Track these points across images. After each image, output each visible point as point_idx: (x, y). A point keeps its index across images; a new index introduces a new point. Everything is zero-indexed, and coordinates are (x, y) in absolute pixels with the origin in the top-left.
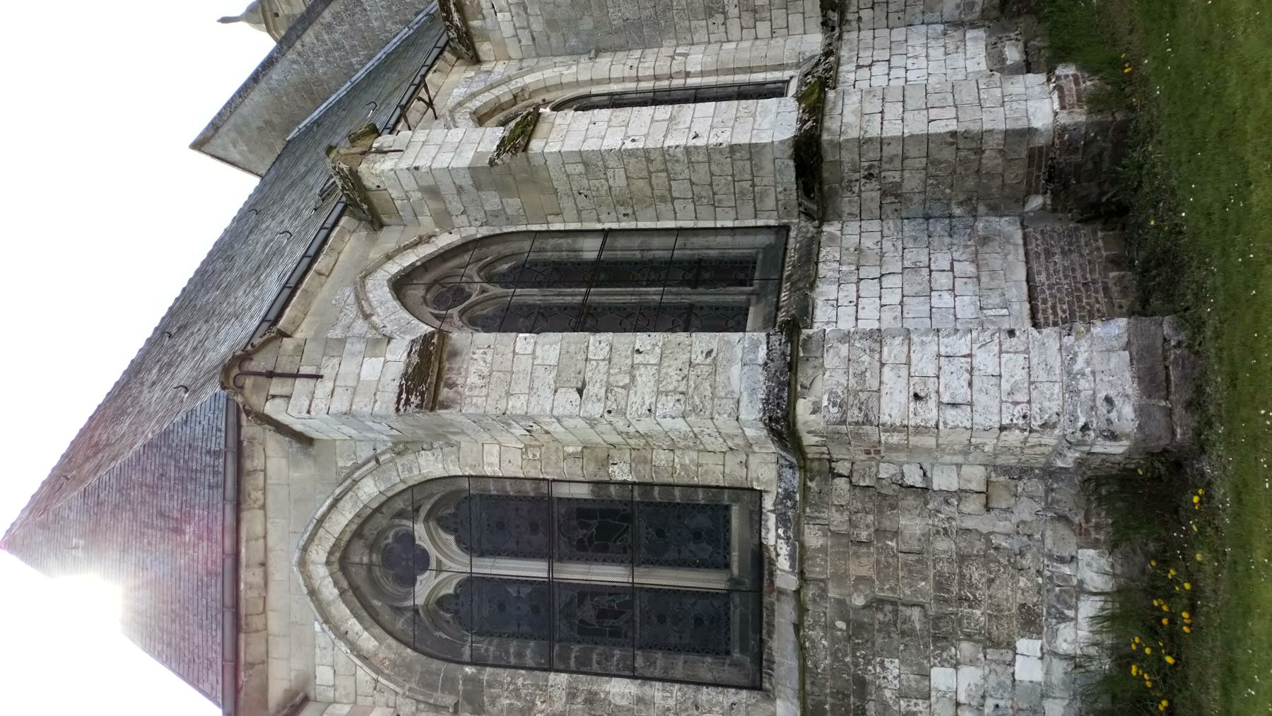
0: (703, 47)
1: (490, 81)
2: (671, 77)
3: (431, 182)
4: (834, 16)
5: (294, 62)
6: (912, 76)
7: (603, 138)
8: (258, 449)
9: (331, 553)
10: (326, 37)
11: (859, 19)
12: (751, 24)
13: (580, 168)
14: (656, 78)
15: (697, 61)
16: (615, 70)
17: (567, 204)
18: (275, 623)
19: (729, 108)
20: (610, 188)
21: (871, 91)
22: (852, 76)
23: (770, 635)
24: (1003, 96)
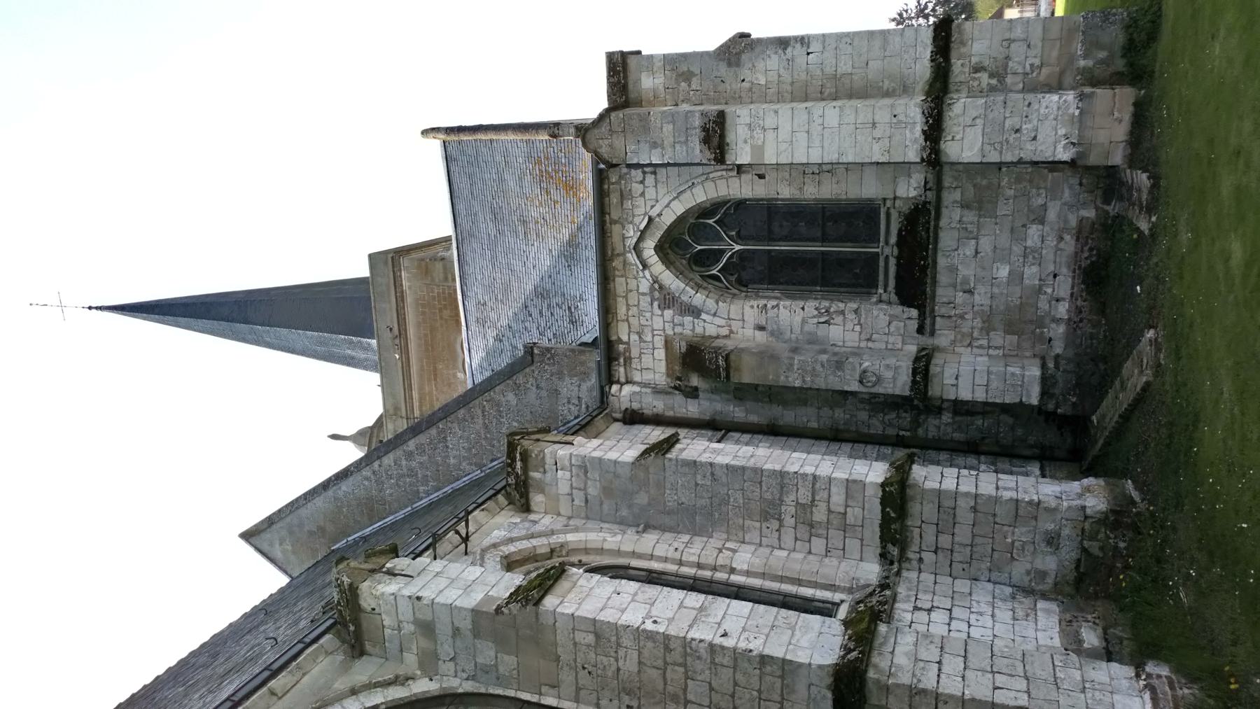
0: (753, 548)
1: (532, 530)
2: (714, 569)
3: (429, 617)
4: (895, 551)
5: (367, 479)
6: (975, 633)
7: (623, 611)
10: (404, 463)
11: (921, 560)
12: (806, 537)
13: (590, 638)
14: (699, 566)
15: (745, 560)
16: (659, 548)
17: (567, 677)
19: (767, 614)
20: (618, 669)
21: (927, 636)
22: (908, 616)
24: (1084, 681)
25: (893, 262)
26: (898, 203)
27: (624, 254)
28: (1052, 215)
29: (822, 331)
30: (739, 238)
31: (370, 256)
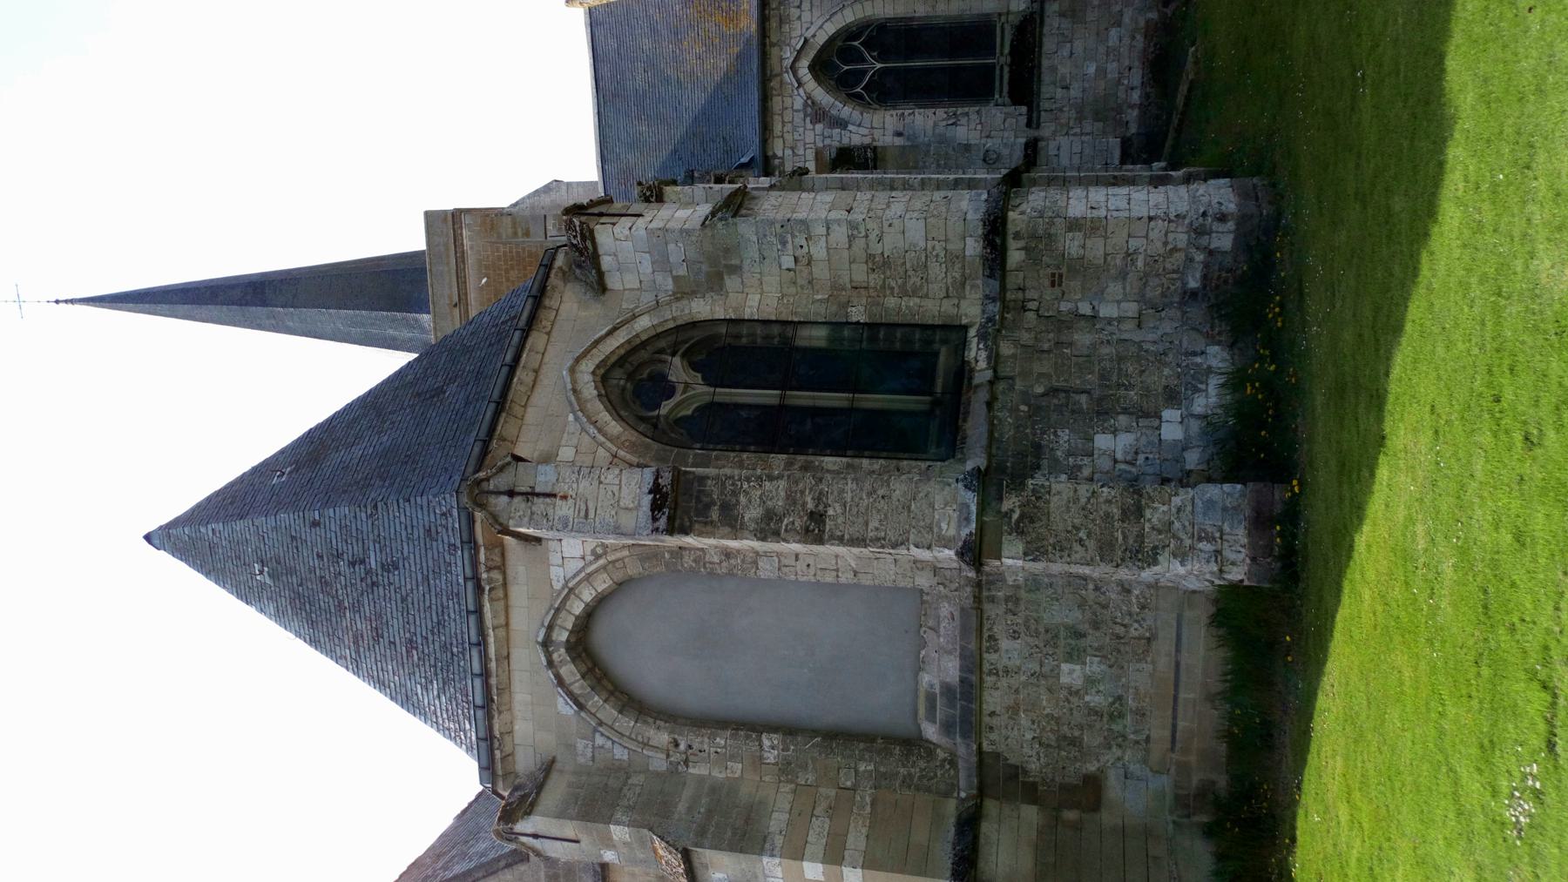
8: (557, 295)
9: (598, 367)
18: (531, 415)
23: (965, 421)
25: (1006, 69)
26: (1011, 18)
27: (780, 75)
28: (1126, 19)
29: (950, 132)
30: (879, 59)
31: (426, 213)
